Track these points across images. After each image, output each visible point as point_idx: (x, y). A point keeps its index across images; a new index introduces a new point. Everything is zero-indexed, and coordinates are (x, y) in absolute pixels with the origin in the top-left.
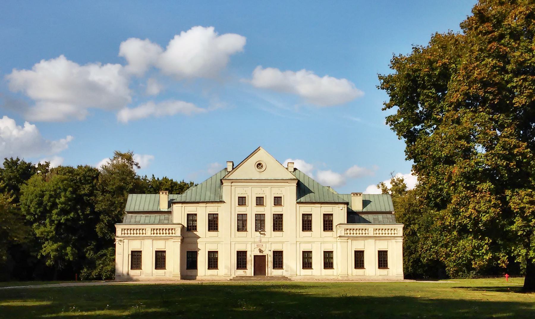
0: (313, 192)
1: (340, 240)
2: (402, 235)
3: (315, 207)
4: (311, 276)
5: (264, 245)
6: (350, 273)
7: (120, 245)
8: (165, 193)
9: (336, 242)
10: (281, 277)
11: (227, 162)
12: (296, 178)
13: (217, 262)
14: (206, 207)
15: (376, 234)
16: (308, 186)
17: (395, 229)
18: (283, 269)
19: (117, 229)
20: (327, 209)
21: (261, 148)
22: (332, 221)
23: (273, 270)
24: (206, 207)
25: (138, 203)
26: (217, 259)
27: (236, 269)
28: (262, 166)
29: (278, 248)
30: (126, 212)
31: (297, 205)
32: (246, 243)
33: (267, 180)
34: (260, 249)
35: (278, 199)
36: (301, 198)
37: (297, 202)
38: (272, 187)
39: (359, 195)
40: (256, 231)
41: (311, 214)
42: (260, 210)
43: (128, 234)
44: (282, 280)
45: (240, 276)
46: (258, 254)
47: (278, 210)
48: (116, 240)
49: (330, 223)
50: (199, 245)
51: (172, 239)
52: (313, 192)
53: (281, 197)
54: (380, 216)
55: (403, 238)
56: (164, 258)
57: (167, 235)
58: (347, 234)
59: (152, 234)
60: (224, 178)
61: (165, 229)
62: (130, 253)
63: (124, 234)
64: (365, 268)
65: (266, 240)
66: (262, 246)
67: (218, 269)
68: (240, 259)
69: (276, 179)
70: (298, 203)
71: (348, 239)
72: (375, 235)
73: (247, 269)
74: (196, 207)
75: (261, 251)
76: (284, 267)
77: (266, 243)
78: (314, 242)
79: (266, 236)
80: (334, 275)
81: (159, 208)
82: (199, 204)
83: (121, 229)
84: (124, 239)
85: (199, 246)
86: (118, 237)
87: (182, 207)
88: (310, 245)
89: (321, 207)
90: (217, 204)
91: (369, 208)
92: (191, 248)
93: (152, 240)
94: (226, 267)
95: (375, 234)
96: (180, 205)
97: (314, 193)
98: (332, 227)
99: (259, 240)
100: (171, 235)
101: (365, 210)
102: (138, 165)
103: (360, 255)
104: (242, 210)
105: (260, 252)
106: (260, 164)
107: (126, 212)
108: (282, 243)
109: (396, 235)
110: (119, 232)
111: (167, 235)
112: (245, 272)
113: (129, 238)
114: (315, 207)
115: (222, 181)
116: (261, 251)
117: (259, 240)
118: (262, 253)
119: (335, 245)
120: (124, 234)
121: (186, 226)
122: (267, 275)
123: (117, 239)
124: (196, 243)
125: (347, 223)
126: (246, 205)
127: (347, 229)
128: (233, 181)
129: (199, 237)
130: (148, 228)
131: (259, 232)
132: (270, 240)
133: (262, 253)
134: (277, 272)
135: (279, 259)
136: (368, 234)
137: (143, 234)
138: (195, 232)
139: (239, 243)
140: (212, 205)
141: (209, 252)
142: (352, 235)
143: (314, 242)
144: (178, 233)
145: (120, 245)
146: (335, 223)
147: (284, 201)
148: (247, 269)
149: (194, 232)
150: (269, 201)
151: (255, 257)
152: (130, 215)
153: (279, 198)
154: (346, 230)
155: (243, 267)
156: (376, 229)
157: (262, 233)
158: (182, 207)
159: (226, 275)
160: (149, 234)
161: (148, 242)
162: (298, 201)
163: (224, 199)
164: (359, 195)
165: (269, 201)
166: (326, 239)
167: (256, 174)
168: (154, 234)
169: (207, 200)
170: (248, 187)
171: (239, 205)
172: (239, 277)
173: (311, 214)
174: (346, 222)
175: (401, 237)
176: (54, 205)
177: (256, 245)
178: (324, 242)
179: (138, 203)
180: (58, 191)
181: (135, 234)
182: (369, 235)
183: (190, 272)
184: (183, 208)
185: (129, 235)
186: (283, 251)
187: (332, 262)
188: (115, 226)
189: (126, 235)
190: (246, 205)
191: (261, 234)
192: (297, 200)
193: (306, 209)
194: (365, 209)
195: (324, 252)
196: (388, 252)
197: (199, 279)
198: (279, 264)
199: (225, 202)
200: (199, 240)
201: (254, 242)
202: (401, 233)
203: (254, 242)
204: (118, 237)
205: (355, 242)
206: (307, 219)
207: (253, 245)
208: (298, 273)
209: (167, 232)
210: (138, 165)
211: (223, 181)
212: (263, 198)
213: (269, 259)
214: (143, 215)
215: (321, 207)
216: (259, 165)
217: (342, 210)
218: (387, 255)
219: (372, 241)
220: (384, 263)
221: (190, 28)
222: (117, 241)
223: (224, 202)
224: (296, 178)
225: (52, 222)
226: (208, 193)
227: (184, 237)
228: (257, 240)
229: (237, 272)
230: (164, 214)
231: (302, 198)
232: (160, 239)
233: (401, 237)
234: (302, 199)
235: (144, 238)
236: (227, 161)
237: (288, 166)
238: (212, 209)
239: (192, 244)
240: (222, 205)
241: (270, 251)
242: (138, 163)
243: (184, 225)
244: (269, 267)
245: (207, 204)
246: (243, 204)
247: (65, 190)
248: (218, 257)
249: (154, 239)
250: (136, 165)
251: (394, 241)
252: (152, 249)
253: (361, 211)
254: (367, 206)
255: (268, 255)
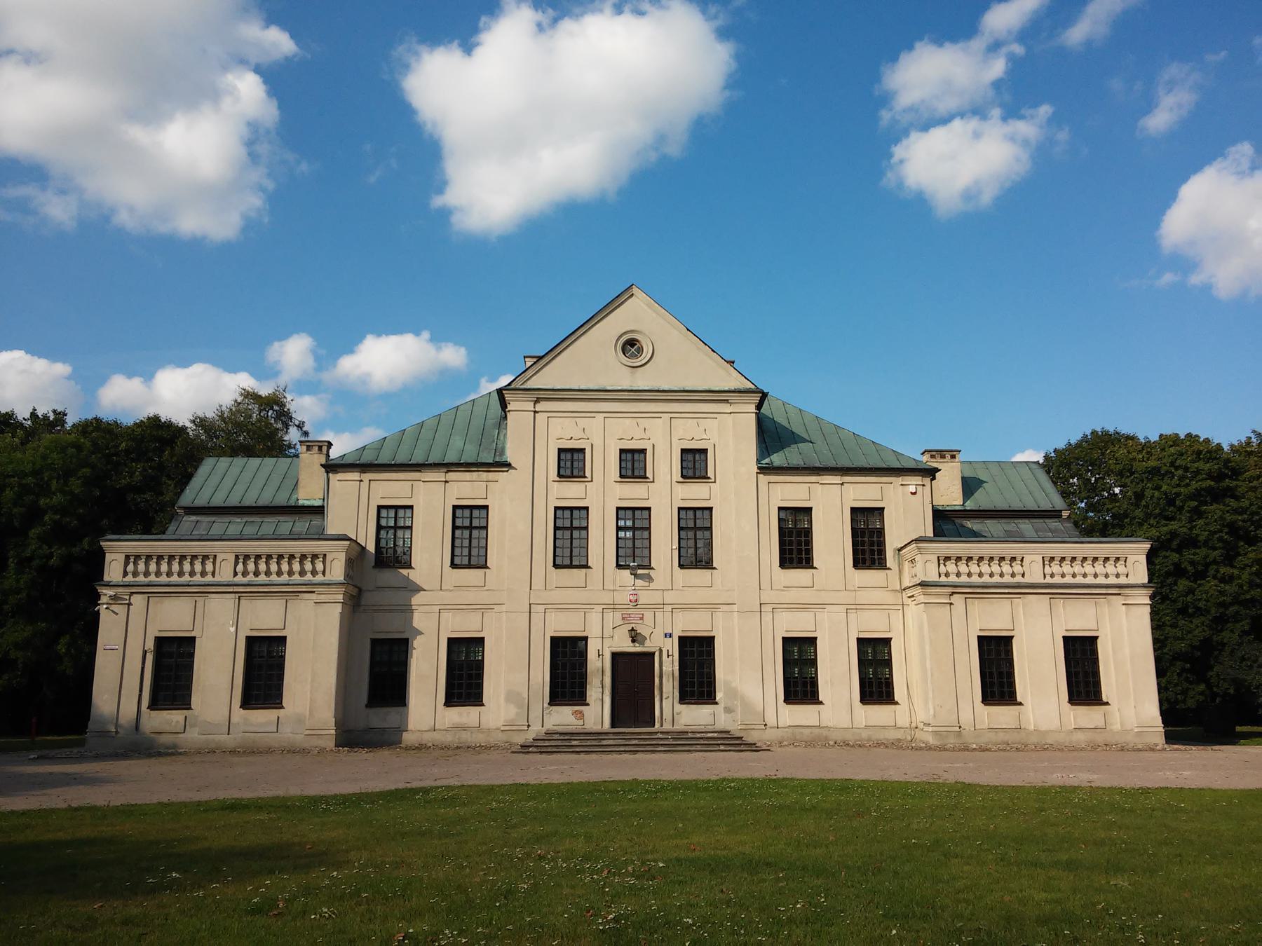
0: (804, 440)
1: (922, 599)
2: (1144, 579)
3: (821, 484)
4: (817, 731)
5: (648, 615)
6: (966, 718)
7: (117, 614)
8: (317, 448)
9: (901, 607)
10: (716, 735)
11: (525, 357)
12: (753, 387)
13: (480, 676)
14: (446, 482)
15: (1052, 576)
16: (785, 423)
17: (1118, 559)
18: (717, 703)
19: (108, 557)
20: (864, 492)
21: (635, 290)
22: (881, 532)
23: (678, 707)
24: (446, 482)
25: (228, 482)
26: (480, 666)
27: (546, 705)
28: (640, 350)
29: (695, 625)
30: (180, 508)
31: (761, 476)
32: (584, 609)
33: (658, 391)
34: (633, 629)
35: (694, 458)
36: (772, 457)
37: (759, 468)
38: (674, 416)
39: (948, 456)
40: (619, 566)
41: (810, 509)
42: (633, 494)
43: (147, 574)
44: (722, 748)
45: (561, 734)
46: (628, 646)
47: (695, 494)
48: (102, 597)
49: (875, 539)
50: (416, 616)
51: (313, 592)
52: (805, 436)
53: (705, 451)
54: (1026, 526)
55: (1150, 591)
56: (277, 666)
57: (296, 577)
58: (947, 575)
59: (240, 575)
60: (509, 384)
61: (286, 557)
62: (150, 645)
63: (135, 574)
64: (1019, 699)
65: (656, 598)
66: (642, 619)
67: (483, 705)
68: (564, 665)
69: (687, 389)
70: (764, 470)
71: (953, 593)
72: (1049, 580)
73: (588, 705)
74: (411, 483)
75: (635, 637)
76: (719, 696)
77: (655, 607)
78: (822, 605)
79: (653, 586)
80: (898, 726)
81: (294, 497)
82: (423, 474)
83: (123, 556)
84: (132, 593)
85: (418, 621)
86: (108, 585)
87: (361, 481)
88: (808, 616)
89: (842, 484)
90: (485, 474)
91: (980, 500)
92: (388, 627)
93: (237, 595)
94: (511, 697)
95: (1048, 577)
96: (355, 476)
97: (811, 442)
98: (882, 552)
99: (632, 597)
100: (309, 577)
101: (970, 505)
102: (304, 429)
103: (998, 653)
104: (571, 493)
105: (633, 641)
106: (631, 343)
107: (180, 508)
108: (712, 607)
109: (1123, 580)
110: (114, 569)
111: (296, 577)
112: (581, 712)
113: (152, 591)
114: (821, 484)
115: (503, 395)
116: (635, 637)
117: (632, 597)
118: (642, 643)
119: (896, 618)
120: (135, 574)
121: (371, 548)
122: (657, 725)
123: (106, 593)
124: (408, 610)
125: (935, 535)
126: (585, 477)
127: (947, 559)
128: (541, 396)
129: (418, 589)
130: (225, 553)
131: (628, 572)
132: (670, 597)
133: (642, 643)
134: (695, 716)
135: (701, 666)
136: (1023, 575)
137: (203, 574)
138: (404, 572)
139: (562, 608)
140: (467, 476)
141: (451, 641)
142: (964, 579)
143: (822, 605)
144: (337, 571)
145: (117, 614)
146: (893, 540)
147: (719, 464)
148: (588, 705)
149: (401, 570)
150: (665, 465)
151: (616, 656)
152: (193, 518)
153: (697, 456)
154: (942, 562)
155: (573, 695)
156: (1052, 559)
157: (640, 572)
158: (361, 481)
159: (511, 727)
160: (225, 572)
161: (220, 608)
162: (764, 462)
163: (510, 456)
164: (948, 456)
165: (665, 465)
166: (865, 597)
167: (619, 375)
168: (245, 574)
169: (451, 457)
170: (593, 415)
171: (559, 475)
172: (556, 737)
173: (810, 509)
174: (930, 533)
175: (1144, 586)
176: (34, 515)
177: (618, 615)
178: (858, 607)
179: (228, 482)
180: (46, 476)
181: (175, 576)
182: (1027, 580)
183: (382, 718)
184: (365, 485)
185: (152, 578)
186: (713, 638)
187: (812, 678)
188: (101, 543)
189: (141, 578)
190: (585, 477)
191: (636, 576)
192: (758, 461)
193: (793, 491)
194: (968, 502)
195: (860, 641)
196: (1099, 641)
197: (409, 744)
198: (701, 684)
199: (513, 465)
200: (417, 599)
201: (614, 607)
202: (1138, 570)
203: (614, 607)
204: (108, 585)
205: (976, 606)
206: (795, 524)
207: (609, 616)
208: (771, 720)
209: (296, 567)
210: (304, 429)
211: (508, 396)
212: (642, 455)
213: (667, 668)
214: (239, 520)
215: (842, 484)
216: (630, 346)
217: (915, 493)
218: (1094, 652)
219: (1038, 604)
220: (1001, 685)
221: (498, 378)
222: (104, 599)
223: (509, 465)
224: (753, 387)
225: (23, 563)
226: (457, 442)
227: (364, 588)
228: (623, 597)
229: (550, 713)
230: (309, 517)
231: (775, 455)
232: (267, 592)
233: (1144, 586)
234: (777, 459)
235: (205, 590)
236: (526, 355)
237: (528, 722)
238: (466, 488)
239: (391, 611)
240: (502, 477)
241: (670, 636)
242: (304, 422)
243: (364, 545)
244: (664, 697)
245: (450, 474)
246: (575, 473)
247: (67, 474)
248: (483, 660)
249: (242, 592)
250: (300, 427)
251: (1120, 600)
252: (233, 629)
253: (961, 508)
254: (975, 495)
255: (661, 651)
